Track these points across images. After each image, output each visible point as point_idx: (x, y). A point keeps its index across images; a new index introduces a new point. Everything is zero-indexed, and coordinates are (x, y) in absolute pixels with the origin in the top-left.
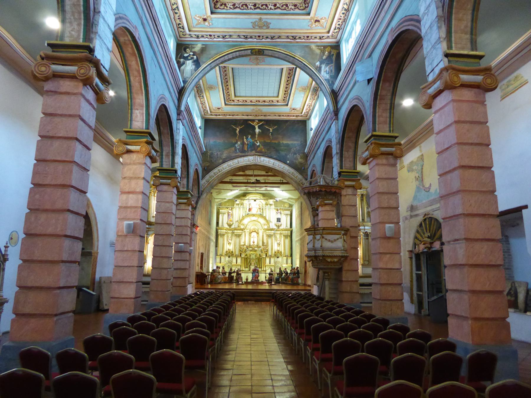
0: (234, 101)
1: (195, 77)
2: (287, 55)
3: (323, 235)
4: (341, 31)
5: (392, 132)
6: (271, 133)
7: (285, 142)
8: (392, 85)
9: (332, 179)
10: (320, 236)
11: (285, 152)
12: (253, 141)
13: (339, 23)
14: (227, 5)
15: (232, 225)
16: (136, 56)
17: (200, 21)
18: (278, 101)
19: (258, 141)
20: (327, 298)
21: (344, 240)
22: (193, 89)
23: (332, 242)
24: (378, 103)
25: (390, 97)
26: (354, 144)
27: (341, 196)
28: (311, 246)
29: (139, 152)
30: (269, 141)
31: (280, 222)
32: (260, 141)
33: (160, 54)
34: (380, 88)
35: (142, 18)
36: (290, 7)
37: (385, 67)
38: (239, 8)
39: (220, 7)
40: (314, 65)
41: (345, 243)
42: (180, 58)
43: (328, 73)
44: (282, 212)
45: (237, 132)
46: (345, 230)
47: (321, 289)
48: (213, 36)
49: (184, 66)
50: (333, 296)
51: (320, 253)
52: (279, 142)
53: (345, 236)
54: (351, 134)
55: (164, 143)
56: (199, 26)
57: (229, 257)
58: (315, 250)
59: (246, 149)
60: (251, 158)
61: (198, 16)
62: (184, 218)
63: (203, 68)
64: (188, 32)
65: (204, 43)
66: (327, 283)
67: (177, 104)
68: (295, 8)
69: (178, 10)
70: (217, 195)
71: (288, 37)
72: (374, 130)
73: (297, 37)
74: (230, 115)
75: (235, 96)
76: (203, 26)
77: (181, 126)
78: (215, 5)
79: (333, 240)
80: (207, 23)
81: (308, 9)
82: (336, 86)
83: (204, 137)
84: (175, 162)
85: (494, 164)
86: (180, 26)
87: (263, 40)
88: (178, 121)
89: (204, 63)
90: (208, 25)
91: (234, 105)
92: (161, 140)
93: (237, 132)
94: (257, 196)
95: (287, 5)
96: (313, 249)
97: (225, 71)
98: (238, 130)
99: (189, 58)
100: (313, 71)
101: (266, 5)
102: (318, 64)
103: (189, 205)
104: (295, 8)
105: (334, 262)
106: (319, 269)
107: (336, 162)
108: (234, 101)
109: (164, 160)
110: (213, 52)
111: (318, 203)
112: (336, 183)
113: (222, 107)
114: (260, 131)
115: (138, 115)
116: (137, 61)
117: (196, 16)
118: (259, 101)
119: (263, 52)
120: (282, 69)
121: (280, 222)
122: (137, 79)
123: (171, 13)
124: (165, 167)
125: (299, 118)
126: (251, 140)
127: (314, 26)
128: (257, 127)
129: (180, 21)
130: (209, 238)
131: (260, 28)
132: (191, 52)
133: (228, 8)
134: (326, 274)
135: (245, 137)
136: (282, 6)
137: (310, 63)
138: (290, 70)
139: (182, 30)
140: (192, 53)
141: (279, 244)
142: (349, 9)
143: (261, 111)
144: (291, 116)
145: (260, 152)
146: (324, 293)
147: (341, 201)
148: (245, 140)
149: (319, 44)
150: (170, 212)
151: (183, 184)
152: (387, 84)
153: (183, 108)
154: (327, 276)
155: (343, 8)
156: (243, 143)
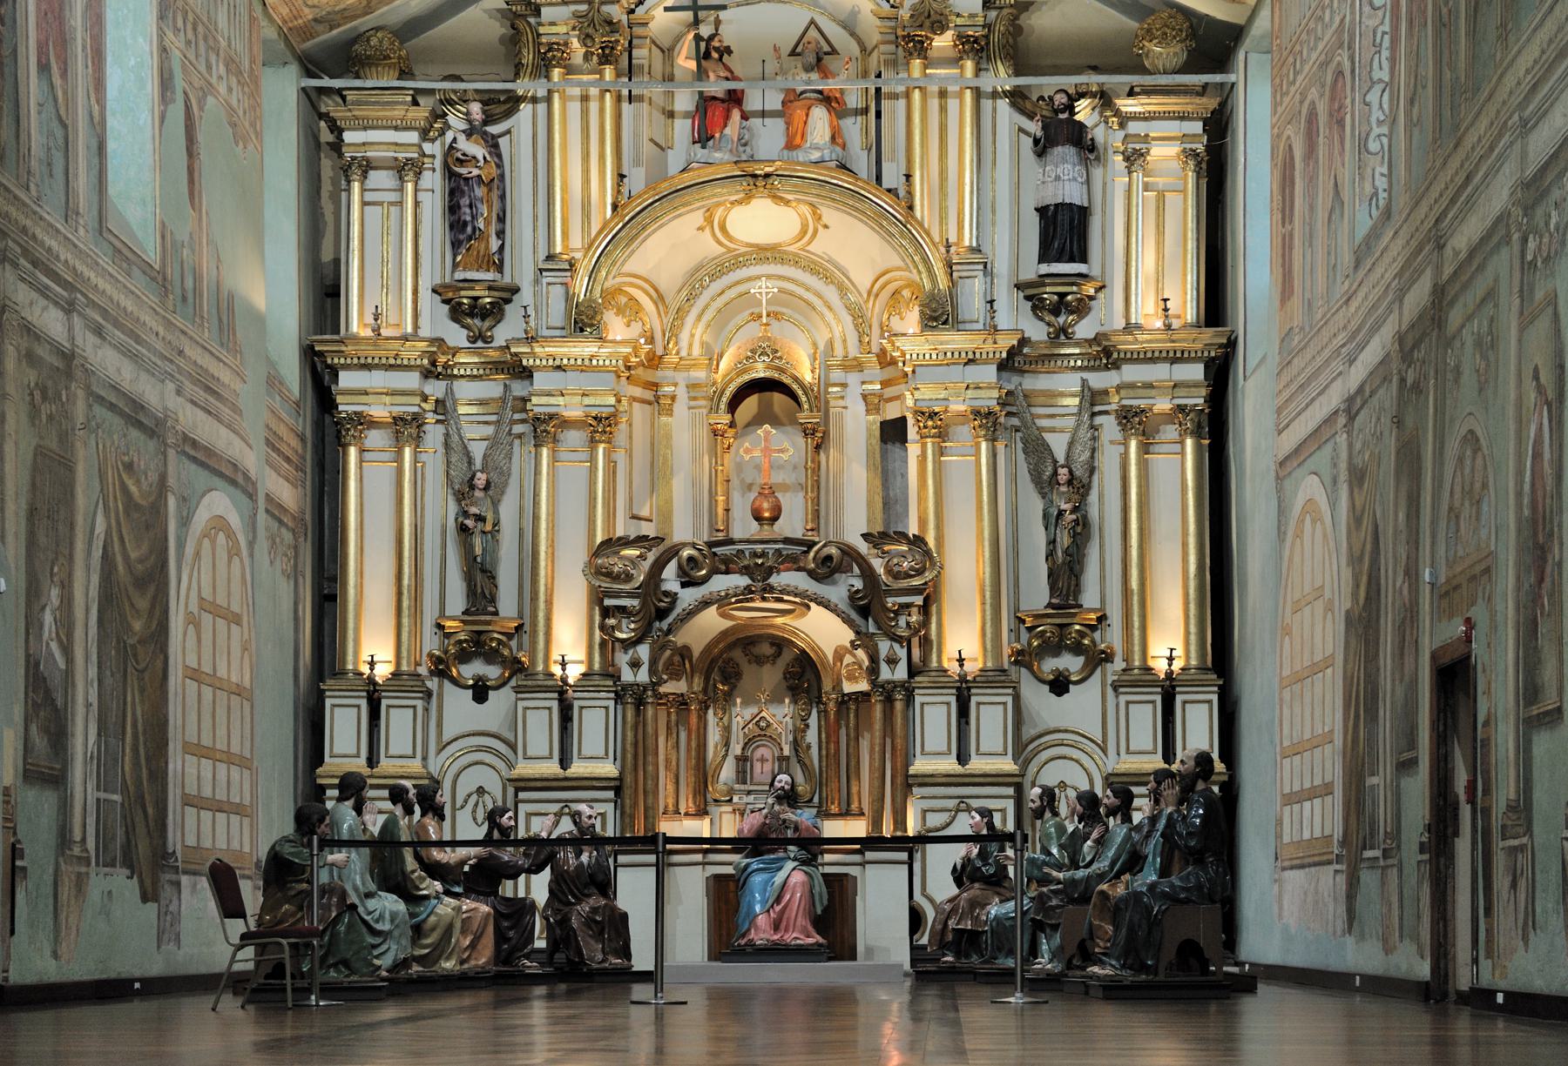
57: (480, 692)
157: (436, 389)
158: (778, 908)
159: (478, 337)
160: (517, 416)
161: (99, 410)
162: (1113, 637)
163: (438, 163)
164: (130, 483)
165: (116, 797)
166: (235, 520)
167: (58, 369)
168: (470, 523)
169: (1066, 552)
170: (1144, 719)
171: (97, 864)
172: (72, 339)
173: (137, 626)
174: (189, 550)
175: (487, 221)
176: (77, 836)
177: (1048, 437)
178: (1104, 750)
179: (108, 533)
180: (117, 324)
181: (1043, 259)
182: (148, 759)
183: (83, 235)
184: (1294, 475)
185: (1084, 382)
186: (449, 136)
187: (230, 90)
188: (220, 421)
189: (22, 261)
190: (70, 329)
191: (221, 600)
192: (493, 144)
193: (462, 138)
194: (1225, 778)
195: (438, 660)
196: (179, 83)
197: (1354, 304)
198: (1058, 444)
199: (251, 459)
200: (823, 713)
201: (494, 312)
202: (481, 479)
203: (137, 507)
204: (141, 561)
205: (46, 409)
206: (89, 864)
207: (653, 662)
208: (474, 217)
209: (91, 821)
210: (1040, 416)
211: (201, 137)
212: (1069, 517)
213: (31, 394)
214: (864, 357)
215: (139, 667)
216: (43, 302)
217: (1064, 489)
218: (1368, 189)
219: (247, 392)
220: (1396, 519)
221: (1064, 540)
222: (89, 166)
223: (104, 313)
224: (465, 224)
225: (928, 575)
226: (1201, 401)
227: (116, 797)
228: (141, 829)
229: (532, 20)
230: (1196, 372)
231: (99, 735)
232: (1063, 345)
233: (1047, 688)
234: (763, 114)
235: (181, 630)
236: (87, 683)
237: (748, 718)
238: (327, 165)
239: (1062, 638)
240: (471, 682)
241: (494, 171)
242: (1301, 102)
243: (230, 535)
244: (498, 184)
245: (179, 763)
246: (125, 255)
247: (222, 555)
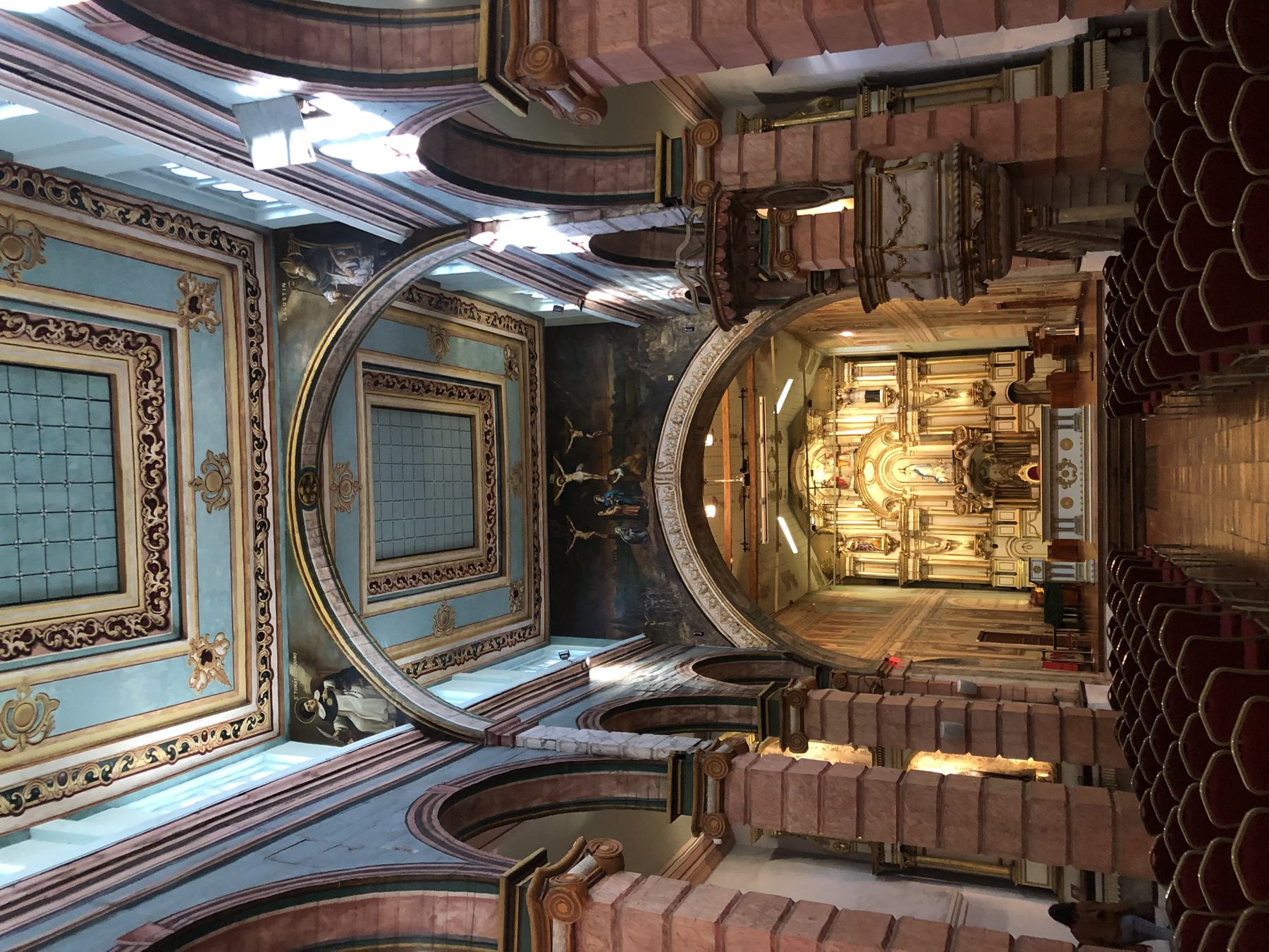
0: (491, 549)
1: (386, 684)
2: (309, 396)
3: (884, 244)
4: (223, 227)
5: (477, 11)
6: (585, 433)
7: (611, 391)
8: (312, 22)
9: (688, 229)
10: (886, 256)
11: (643, 388)
12: (610, 487)
13: (196, 236)
14: (155, 589)
15: (891, 539)
16: (240, 928)
17: (213, 673)
18: (486, 417)
19: (612, 472)
20: (1125, 211)
21: (901, 165)
22: (423, 690)
23: (908, 210)
24: (379, 71)
25: (357, 29)
26: (569, 160)
27: (744, 192)
28: (927, 286)
29: (574, 926)
30: (610, 438)
31: (878, 392)
32: (610, 465)
33: (269, 820)
34: (325, 66)
35: (112, 905)
36: (152, 393)
37: (245, 51)
38: (161, 552)
39: (163, 612)
40: (335, 309)
41: (911, 162)
42: (332, 731)
43: (357, 261)
44: (847, 387)
45: (585, 536)
46: (865, 166)
47: (1091, 237)
48: (262, 630)
49: (352, 719)
50: (1120, 190)
51: (951, 250)
52: (613, 408)
53: (887, 165)
54: (536, 174)
55: (585, 794)
56: (229, 674)
57: (995, 546)
58: (940, 269)
59: (636, 509)
60: (662, 493)
61: (193, 680)
62: (850, 718)
63: (357, 660)
64: (251, 708)
65: (286, 655)
66: (1066, 217)
67: (466, 747)
68: (156, 377)
69: (174, 742)
70: (796, 585)
71: (256, 396)
72: (471, 75)
73: (255, 366)
74: (537, 560)
75: (474, 546)
76: (228, 661)
77: (533, 736)
78: (155, 627)
79: (900, 208)
80: (219, 651)
81: (159, 338)
82: (394, 234)
83: (604, 637)
84: (648, 758)
85: (890, 48)
86: (230, 732)
87: (269, 471)
88: (519, 743)
89: (342, 656)
90: (225, 645)
91: (502, 548)
92: (574, 804)
93: (585, 536)
94: (798, 465)
95: (146, 404)
96: (937, 276)
97: (388, 582)
98: (579, 534)
99: (330, 702)
100: (354, 313)
101: (149, 468)
102: (330, 297)
103: (807, 699)
104: (156, 377)
105: (984, 196)
106: (1013, 251)
107: (632, 220)
108: (491, 549)
109: (643, 796)
110: (311, 628)
111: (789, 275)
112: (699, 211)
113: (511, 585)
114: (579, 468)
115: (451, 915)
116: (257, 924)
117: (193, 686)
118: (488, 474)
119: (306, 470)
120: (373, 406)
121: (878, 392)
122: (324, 919)
123: (183, 763)
124: (665, 794)
125: (539, 349)
126: (608, 494)
127: (211, 315)
128: (568, 478)
129: (213, 734)
130: (936, 608)
131: (226, 482)
132: (312, 696)
133: (165, 586)
134: (1034, 223)
135: (601, 513)
136: (151, 417)
137: (331, 322)
138: (376, 383)
139: (245, 725)
140: (317, 695)
141: (951, 393)
142: (141, 203)
143: (521, 466)
144: (533, 375)
145: (643, 465)
146: (1109, 224)
147: (766, 190)
148: (609, 512)
149: (272, 298)
150: (815, 785)
151: (739, 715)
152: (310, 41)
153: (479, 726)
154: (1039, 221)
155: (139, 223)
156: (619, 518)
162: (980, 380)
181: (878, 401)
230: (909, 362)
244: (859, 538)
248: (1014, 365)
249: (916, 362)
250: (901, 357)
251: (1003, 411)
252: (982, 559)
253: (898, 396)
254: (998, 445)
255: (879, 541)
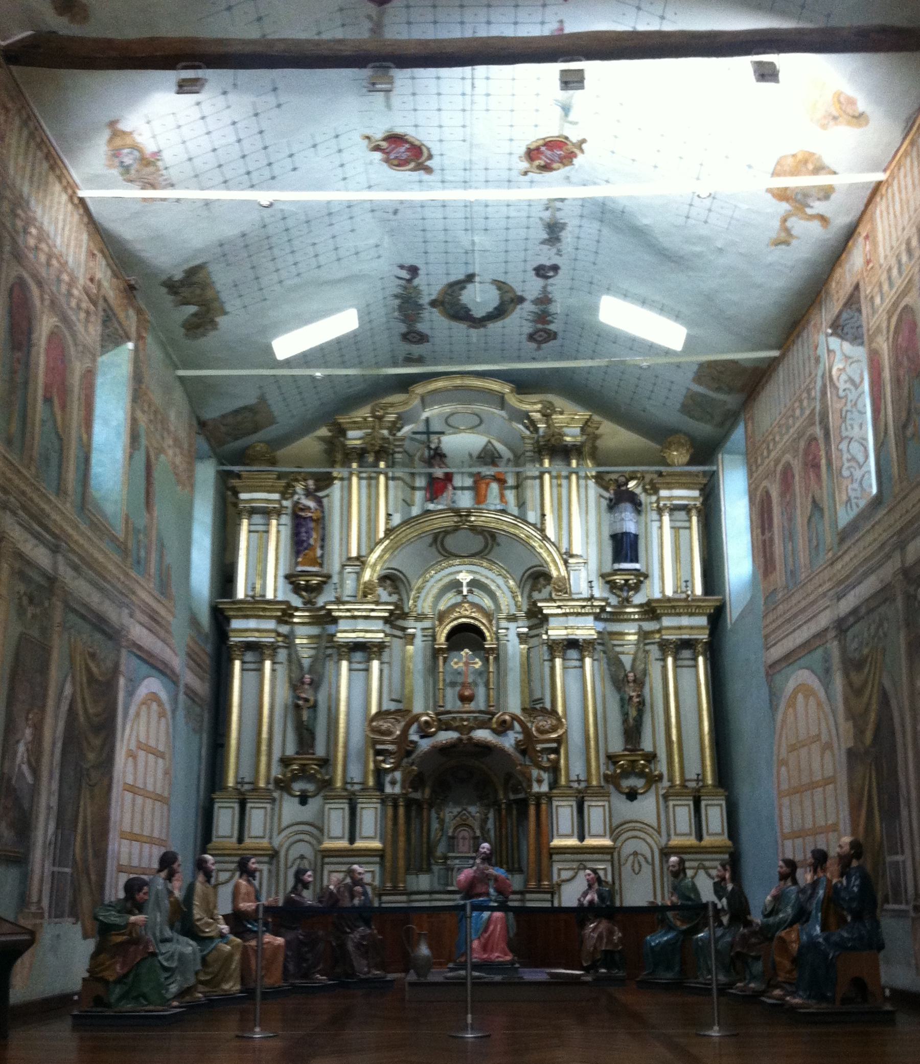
57: (304, 799)
157: (284, 629)
158: (486, 935)
159: (309, 603)
160: (329, 645)
161: (72, 617)
162: (662, 767)
163: (289, 511)
164: (93, 666)
165: (67, 870)
166: (163, 696)
167: (42, 586)
168: (301, 702)
169: (634, 719)
170: (683, 814)
171: (50, 917)
172: (55, 569)
173: (91, 756)
174: (132, 711)
175: (316, 540)
176: (35, 899)
177: (622, 657)
178: (659, 833)
179: (74, 695)
180: (90, 567)
182: (93, 842)
183: (68, 508)
184: (783, 671)
185: (640, 627)
186: (296, 497)
187: (175, 455)
188: (159, 637)
189: (20, 512)
190: (55, 564)
191: (152, 743)
192: (319, 501)
193: (303, 497)
194: (732, 850)
195: (281, 781)
196: (144, 441)
197: (839, 566)
198: (627, 660)
199: (177, 662)
200: (499, 811)
201: (318, 589)
202: (307, 678)
203: (97, 681)
204: (97, 715)
205: (30, 611)
206: (42, 917)
207: (403, 781)
208: (308, 538)
209: (46, 888)
210: (615, 645)
211: (156, 474)
212: (636, 700)
213: (20, 599)
214: (519, 614)
215: (91, 783)
216: (34, 541)
217: (631, 684)
218: (844, 498)
219: (178, 624)
220: (46, 831)
221: (633, 713)
222: (77, 468)
223: (81, 558)
224: (303, 541)
225: (560, 732)
226: (706, 636)
227: (67, 870)
228: (85, 889)
229: (342, 439)
230: (703, 621)
231: (57, 828)
232: (626, 607)
233: (624, 797)
234: (463, 488)
235: (123, 761)
236: (50, 793)
237: (455, 813)
238: (231, 509)
239: (633, 768)
240: (298, 793)
241: (319, 514)
242: (776, 465)
243: (160, 704)
244: (321, 521)
245: (116, 845)
246: (99, 526)
247: (154, 716)
248: (700, 837)
249: (704, 636)
250: (713, 601)
251: (596, 814)
252: (277, 771)
253: (627, 601)
254: (523, 805)
255: (314, 562)
